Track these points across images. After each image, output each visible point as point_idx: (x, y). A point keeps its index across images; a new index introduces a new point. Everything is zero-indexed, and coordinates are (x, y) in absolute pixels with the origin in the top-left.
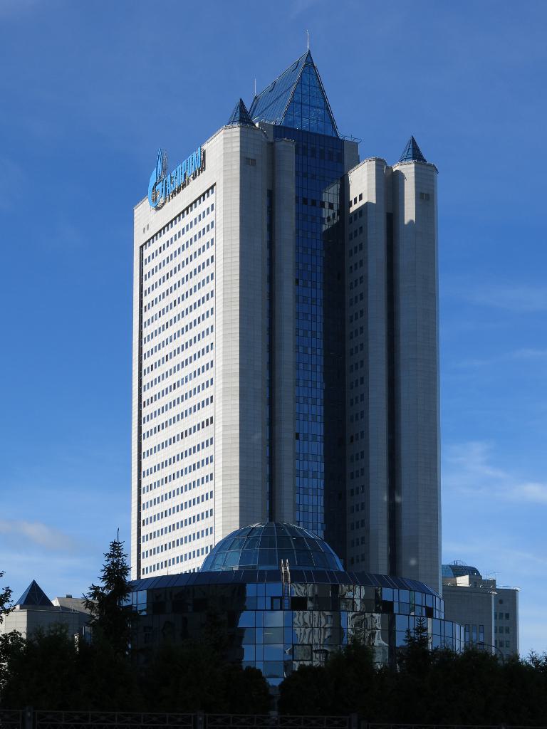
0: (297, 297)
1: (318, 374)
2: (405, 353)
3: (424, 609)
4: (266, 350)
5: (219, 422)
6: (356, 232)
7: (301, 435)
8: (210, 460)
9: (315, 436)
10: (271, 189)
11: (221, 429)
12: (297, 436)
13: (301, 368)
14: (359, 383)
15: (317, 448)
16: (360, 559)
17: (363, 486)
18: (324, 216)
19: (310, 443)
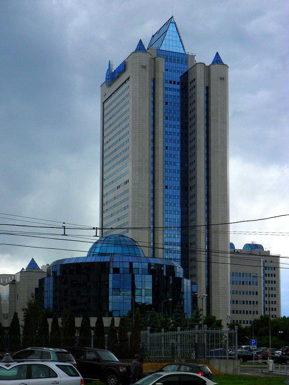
5: (130, 181)
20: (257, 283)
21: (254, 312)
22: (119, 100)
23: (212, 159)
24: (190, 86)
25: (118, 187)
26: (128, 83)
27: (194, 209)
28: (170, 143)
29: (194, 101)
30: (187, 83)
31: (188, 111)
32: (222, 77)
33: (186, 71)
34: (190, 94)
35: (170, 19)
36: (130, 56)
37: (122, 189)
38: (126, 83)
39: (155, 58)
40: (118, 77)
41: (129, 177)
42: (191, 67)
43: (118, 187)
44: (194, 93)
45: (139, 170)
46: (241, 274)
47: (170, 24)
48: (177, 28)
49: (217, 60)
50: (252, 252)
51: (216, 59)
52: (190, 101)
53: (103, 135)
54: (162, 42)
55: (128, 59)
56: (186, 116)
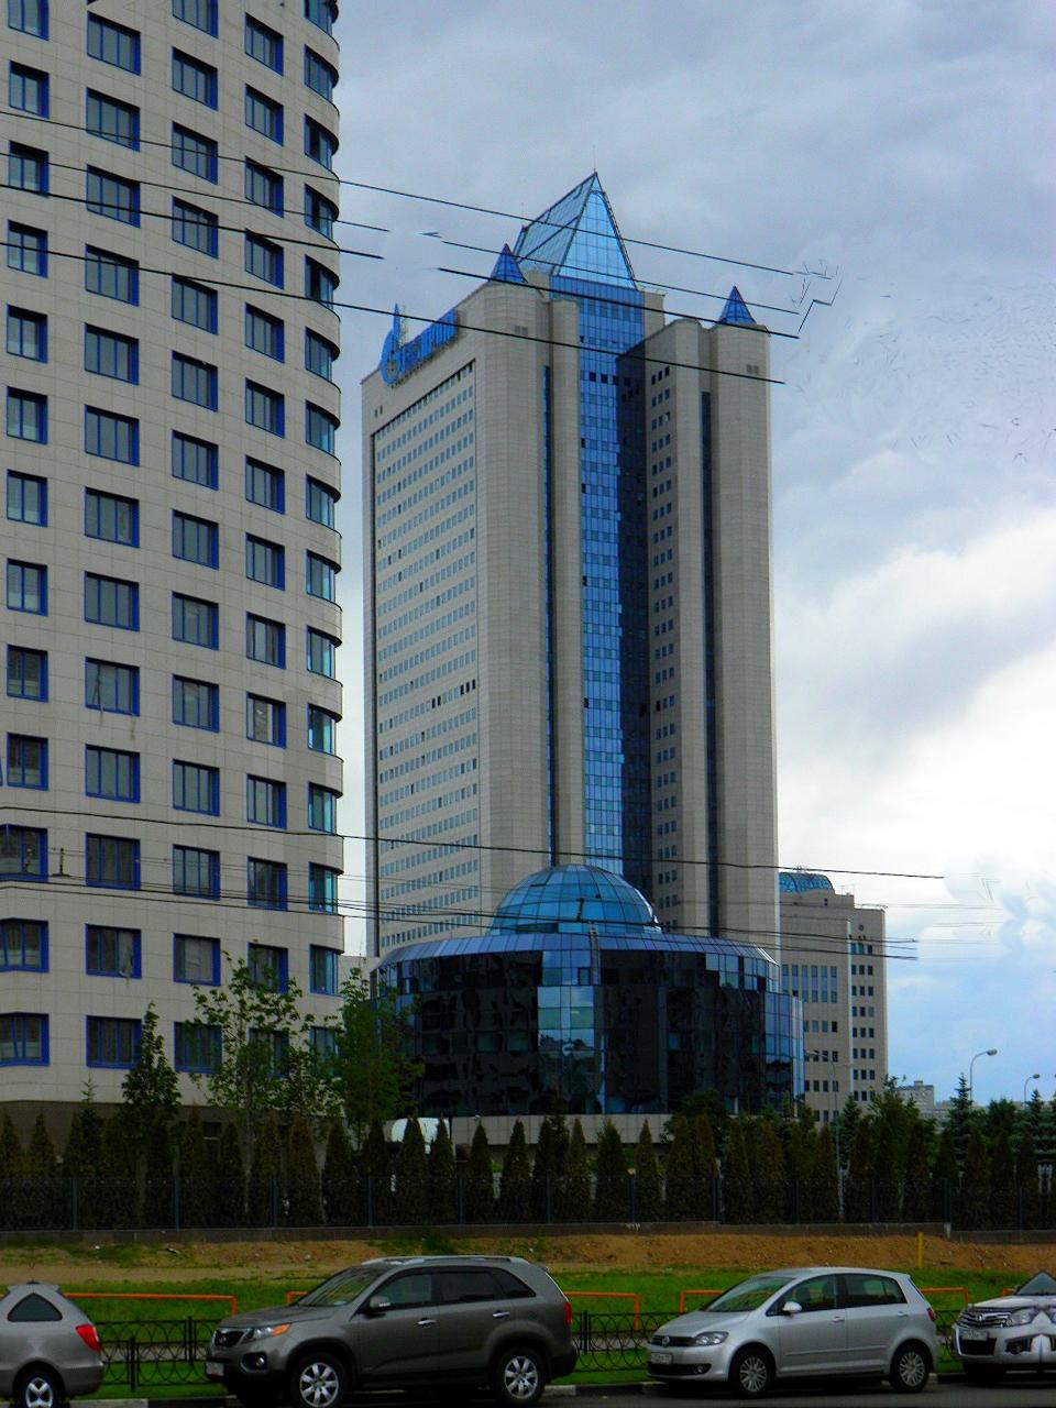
0: (583, 509)
1: (610, 409)
2: (727, 589)
3: (755, 980)
4: (543, 396)
5: (483, 687)
6: (661, 396)
7: (591, 702)
8: (473, 739)
9: (606, 535)
10: (548, 365)
11: (487, 698)
12: (586, 703)
13: (590, 607)
14: (666, 582)
15: (613, 718)
16: (670, 803)
17: (673, 774)
18: (615, 387)
19: (604, 837)
20: (834, 994)
21: (826, 1089)
22: (431, 431)
23: (726, 617)
24: (651, 392)
25: (436, 702)
26: (468, 379)
27: (672, 770)
28: (595, 567)
29: (668, 437)
30: (643, 381)
31: (645, 464)
32: (752, 364)
33: (637, 342)
34: (652, 414)
35: (585, 182)
36: (476, 297)
37: (453, 708)
38: (459, 379)
39: (549, 304)
40: (431, 358)
41: (480, 670)
42: (655, 331)
43: (436, 702)
44: (668, 414)
45: (511, 650)
46: (829, 970)
47: (588, 195)
48: (609, 210)
49: (505, 270)
50: (800, 897)
51: (503, 267)
52: (652, 437)
53: (374, 538)
54: (567, 252)
55: (466, 305)
56: (639, 481)
